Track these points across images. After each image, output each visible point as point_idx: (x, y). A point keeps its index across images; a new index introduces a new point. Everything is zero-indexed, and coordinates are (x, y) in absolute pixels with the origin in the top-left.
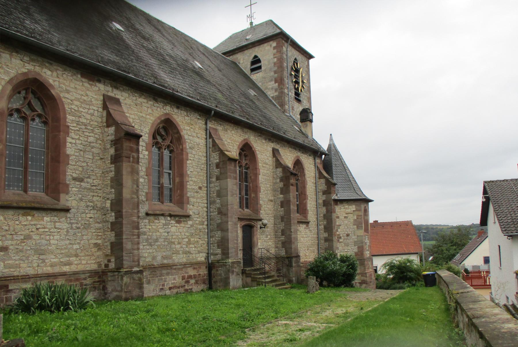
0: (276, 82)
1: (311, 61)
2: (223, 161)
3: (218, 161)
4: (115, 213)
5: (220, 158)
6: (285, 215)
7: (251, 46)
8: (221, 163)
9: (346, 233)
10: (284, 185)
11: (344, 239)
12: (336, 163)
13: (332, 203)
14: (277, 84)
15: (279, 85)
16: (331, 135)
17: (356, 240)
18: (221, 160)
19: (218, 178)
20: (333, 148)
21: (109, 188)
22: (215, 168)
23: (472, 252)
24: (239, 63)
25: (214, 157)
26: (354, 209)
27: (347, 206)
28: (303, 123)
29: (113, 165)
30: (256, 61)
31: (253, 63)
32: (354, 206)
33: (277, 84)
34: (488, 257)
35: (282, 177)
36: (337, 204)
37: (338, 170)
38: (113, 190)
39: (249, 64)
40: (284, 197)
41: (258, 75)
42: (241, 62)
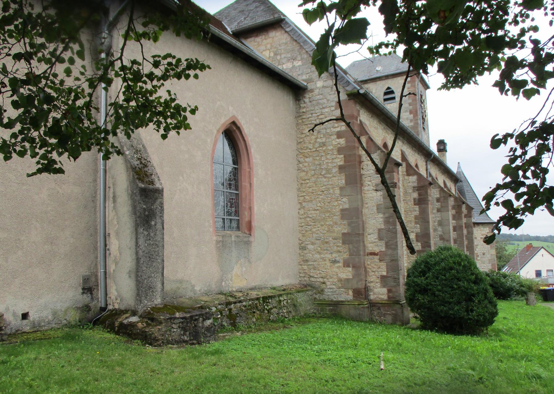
0: (411, 112)
1: (428, 91)
2: (444, 197)
3: (438, 196)
4: (421, 244)
5: (440, 194)
6: (458, 238)
7: (384, 78)
8: (443, 198)
9: (483, 252)
10: (456, 213)
11: (481, 257)
12: (467, 189)
13: (473, 225)
14: (412, 115)
15: (414, 117)
16: (459, 163)
17: (490, 258)
18: (442, 196)
19: (438, 210)
20: (462, 175)
21: (413, 224)
22: (435, 202)
23: (524, 265)
24: (372, 92)
25: (434, 193)
26: (488, 231)
27: (482, 229)
28: (440, 153)
29: (418, 206)
30: (389, 92)
31: (386, 94)
32: (488, 229)
33: (412, 115)
34: (540, 271)
35: (454, 205)
36: (474, 227)
37: (470, 196)
38: (418, 226)
39: (383, 94)
40: (456, 223)
41: (392, 105)
42: (374, 91)
